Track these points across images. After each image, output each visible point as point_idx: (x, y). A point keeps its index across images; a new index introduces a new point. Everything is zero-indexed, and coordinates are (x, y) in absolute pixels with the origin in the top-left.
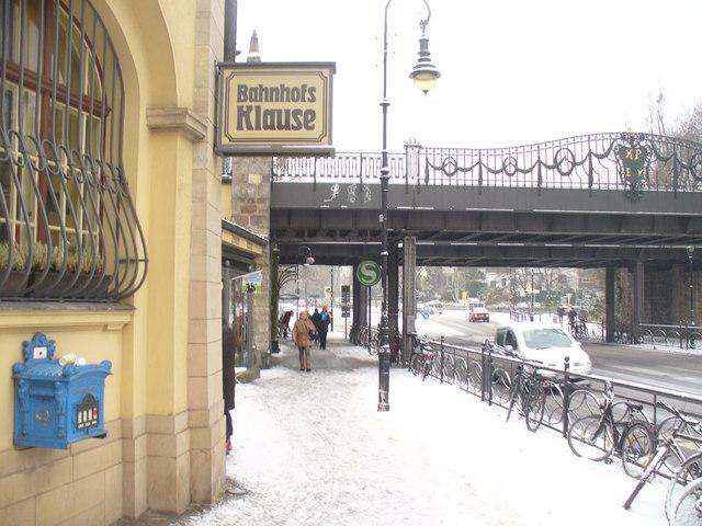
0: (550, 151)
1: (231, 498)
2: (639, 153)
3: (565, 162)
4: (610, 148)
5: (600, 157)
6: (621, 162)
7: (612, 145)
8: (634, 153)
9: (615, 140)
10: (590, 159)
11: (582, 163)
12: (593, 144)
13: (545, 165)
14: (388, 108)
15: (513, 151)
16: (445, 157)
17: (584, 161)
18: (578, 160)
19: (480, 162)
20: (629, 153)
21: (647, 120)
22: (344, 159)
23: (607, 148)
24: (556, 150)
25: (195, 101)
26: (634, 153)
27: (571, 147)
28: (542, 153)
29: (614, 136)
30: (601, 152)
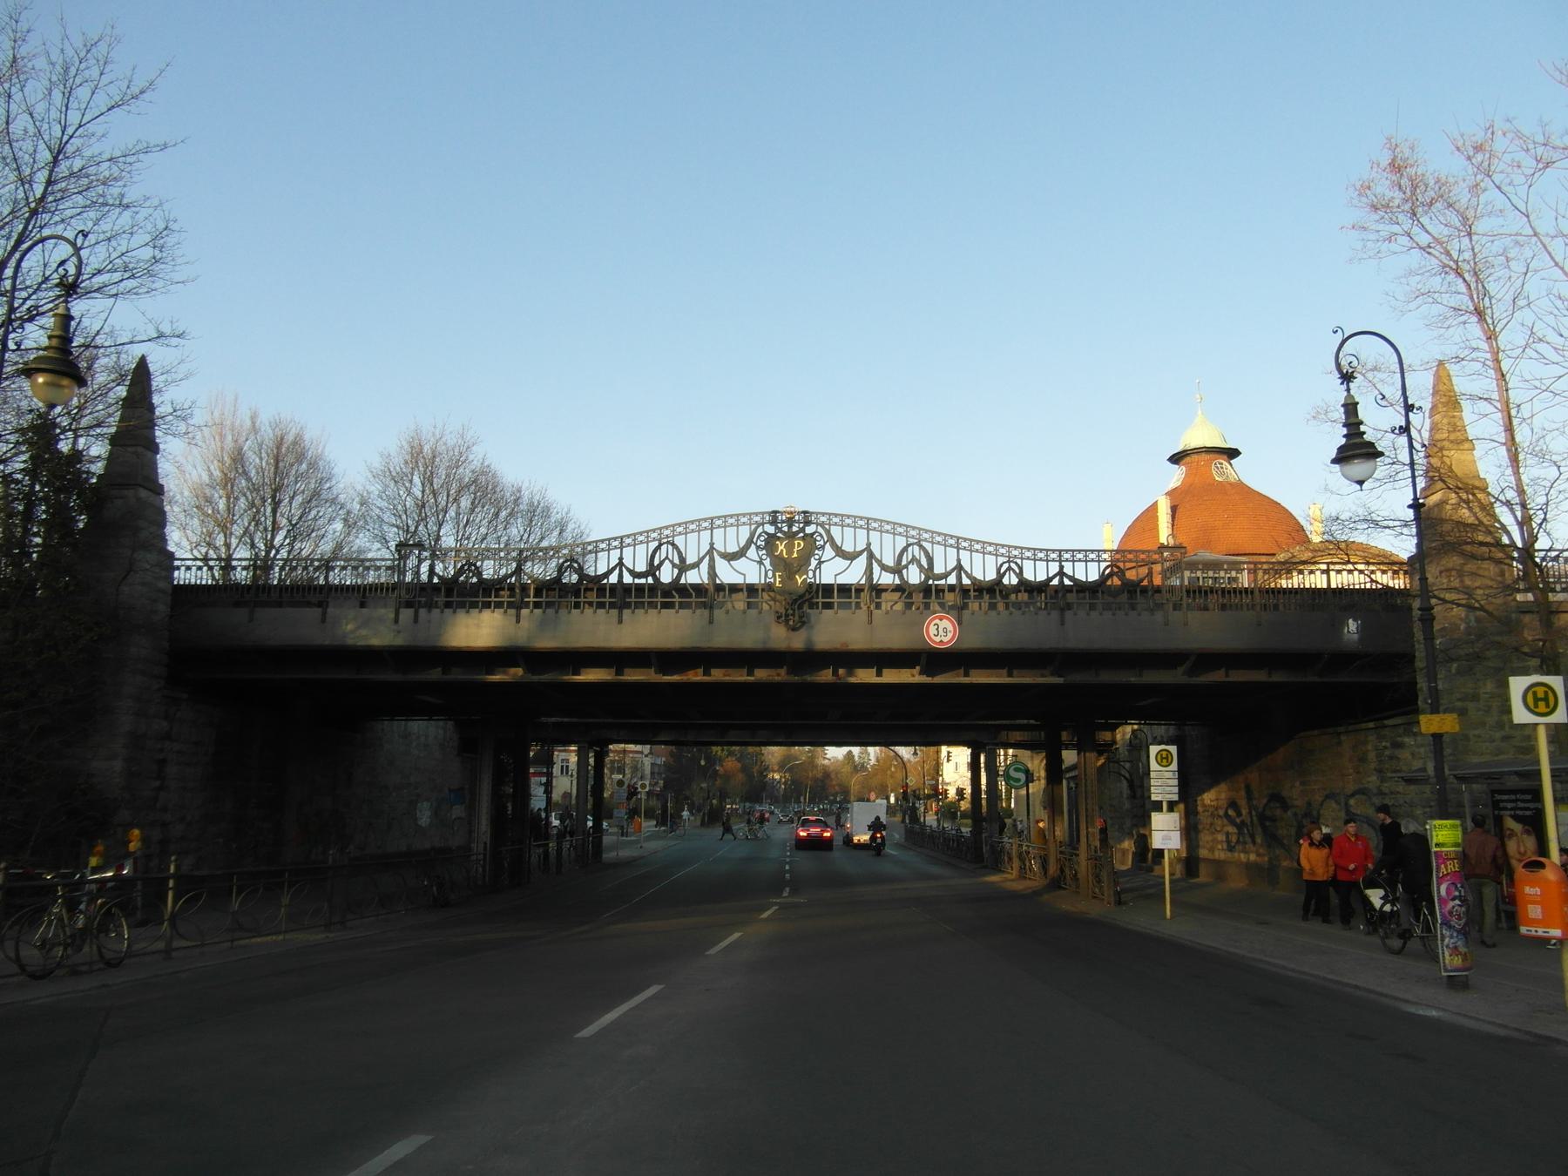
0: (641, 550)
1: (1454, 554)
2: (799, 545)
3: (667, 567)
4: (750, 542)
5: (730, 557)
6: (767, 562)
7: (752, 534)
8: (790, 548)
9: (759, 525)
10: (712, 561)
11: (696, 565)
12: (718, 533)
13: (880, 563)
14: (1338, 437)
15: (1016, 553)
16: (1001, 560)
17: (701, 560)
18: (690, 560)
19: (621, 564)
20: (781, 547)
21: (1544, 336)
22: (194, 569)
23: (742, 543)
24: (654, 545)
25: (1561, 862)
26: (790, 548)
27: (679, 541)
28: (628, 552)
29: (757, 519)
30: (732, 548)
